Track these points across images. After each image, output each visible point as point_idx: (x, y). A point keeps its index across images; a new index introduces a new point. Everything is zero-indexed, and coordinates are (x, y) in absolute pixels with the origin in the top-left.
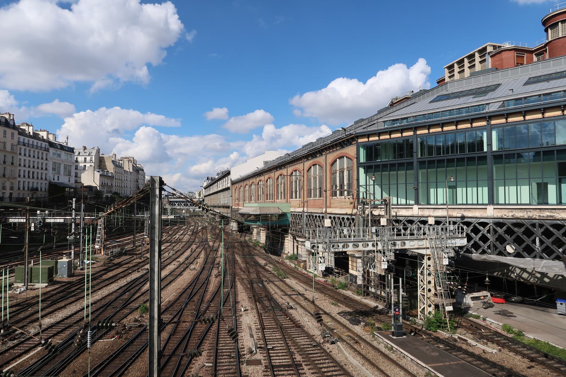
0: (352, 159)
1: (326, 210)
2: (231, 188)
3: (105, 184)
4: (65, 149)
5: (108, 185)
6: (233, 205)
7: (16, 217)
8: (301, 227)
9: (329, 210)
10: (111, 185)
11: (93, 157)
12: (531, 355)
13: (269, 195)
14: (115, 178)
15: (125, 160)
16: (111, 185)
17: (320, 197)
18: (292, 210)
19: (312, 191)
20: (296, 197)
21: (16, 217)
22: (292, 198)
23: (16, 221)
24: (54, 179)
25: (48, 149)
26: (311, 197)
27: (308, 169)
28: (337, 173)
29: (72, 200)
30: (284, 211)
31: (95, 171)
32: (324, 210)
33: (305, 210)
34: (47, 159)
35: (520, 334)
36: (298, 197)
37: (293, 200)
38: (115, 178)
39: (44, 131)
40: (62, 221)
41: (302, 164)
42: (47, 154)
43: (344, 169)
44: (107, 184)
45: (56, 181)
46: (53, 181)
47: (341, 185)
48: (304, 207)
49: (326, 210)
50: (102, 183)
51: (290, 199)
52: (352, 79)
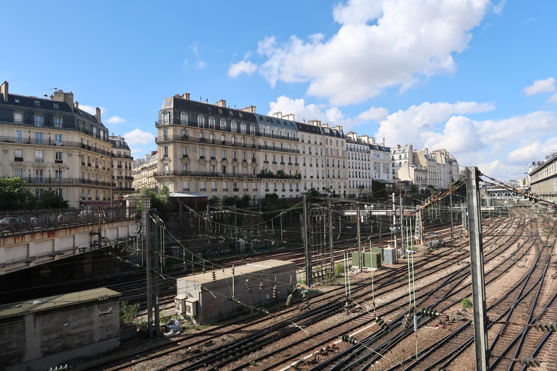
3: (419, 178)
5: (423, 178)
10: (425, 179)
14: (428, 172)
15: (437, 153)
24: (376, 177)
25: (369, 151)
31: (410, 167)
34: (369, 160)
38: (428, 172)
42: (368, 156)
44: (422, 178)
45: (377, 178)
50: (417, 178)
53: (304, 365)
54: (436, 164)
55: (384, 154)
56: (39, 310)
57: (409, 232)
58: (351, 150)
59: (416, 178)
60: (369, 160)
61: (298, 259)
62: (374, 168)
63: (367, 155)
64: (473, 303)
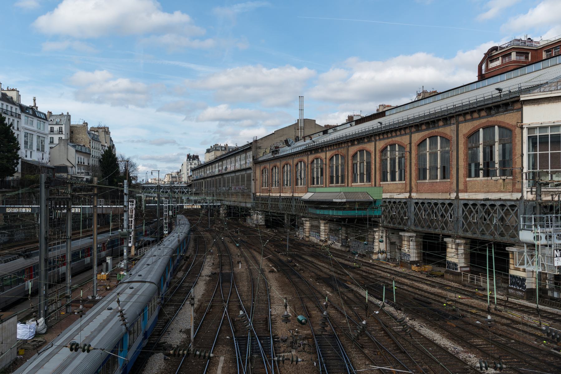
0: (513, 129)
1: (457, 195)
2: (253, 169)
3: (81, 163)
4: (37, 115)
5: (85, 164)
6: (258, 190)
7: (15, 206)
8: (407, 218)
9: (462, 196)
10: (87, 164)
11: (63, 126)
12: (532, 362)
13: (315, 180)
14: (91, 156)
15: (101, 130)
16: (87, 164)
17: (444, 178)
18: (385, 196)
19: (428, 171)
20: (393, 179)
21: (15, 206)
22: (384, 179)
23: (15, 210)
24: (26, 156)
25: (19, 115)
26: (425, 178)
27: (419, 142)
28: (479, 147)
29: (123, 182)
30: (375, 198)
31: (69, 146)
32: (453, 196)
33: (414, 195)
34: (18, 129)
35: (125, 364)
36: (397, 178)
37: (471, 179)
38: (91, 156)
39: (13, 90)
40: (29, 210)
41: (408, 137)
42: (18, 122)
43: (495, 142)
44: (84, 163)
45: (28, 158)
46: (25, 158)
47: (488, 163)
48: (410, 192)
49: (457, 195)
50: (78, 162)
51: (381, 181)
52: (173, 13)
53: (206, 231)
54: (100, 145)
55: (39, 122)
56: (508, 113)
57: (434, 168)
58: (12, 115)
59: (77, 162)
60: (18, 129)
61: (334, 178)
62: (25, 141)
63: (16, 120)
64: (277, 155)
